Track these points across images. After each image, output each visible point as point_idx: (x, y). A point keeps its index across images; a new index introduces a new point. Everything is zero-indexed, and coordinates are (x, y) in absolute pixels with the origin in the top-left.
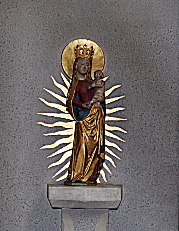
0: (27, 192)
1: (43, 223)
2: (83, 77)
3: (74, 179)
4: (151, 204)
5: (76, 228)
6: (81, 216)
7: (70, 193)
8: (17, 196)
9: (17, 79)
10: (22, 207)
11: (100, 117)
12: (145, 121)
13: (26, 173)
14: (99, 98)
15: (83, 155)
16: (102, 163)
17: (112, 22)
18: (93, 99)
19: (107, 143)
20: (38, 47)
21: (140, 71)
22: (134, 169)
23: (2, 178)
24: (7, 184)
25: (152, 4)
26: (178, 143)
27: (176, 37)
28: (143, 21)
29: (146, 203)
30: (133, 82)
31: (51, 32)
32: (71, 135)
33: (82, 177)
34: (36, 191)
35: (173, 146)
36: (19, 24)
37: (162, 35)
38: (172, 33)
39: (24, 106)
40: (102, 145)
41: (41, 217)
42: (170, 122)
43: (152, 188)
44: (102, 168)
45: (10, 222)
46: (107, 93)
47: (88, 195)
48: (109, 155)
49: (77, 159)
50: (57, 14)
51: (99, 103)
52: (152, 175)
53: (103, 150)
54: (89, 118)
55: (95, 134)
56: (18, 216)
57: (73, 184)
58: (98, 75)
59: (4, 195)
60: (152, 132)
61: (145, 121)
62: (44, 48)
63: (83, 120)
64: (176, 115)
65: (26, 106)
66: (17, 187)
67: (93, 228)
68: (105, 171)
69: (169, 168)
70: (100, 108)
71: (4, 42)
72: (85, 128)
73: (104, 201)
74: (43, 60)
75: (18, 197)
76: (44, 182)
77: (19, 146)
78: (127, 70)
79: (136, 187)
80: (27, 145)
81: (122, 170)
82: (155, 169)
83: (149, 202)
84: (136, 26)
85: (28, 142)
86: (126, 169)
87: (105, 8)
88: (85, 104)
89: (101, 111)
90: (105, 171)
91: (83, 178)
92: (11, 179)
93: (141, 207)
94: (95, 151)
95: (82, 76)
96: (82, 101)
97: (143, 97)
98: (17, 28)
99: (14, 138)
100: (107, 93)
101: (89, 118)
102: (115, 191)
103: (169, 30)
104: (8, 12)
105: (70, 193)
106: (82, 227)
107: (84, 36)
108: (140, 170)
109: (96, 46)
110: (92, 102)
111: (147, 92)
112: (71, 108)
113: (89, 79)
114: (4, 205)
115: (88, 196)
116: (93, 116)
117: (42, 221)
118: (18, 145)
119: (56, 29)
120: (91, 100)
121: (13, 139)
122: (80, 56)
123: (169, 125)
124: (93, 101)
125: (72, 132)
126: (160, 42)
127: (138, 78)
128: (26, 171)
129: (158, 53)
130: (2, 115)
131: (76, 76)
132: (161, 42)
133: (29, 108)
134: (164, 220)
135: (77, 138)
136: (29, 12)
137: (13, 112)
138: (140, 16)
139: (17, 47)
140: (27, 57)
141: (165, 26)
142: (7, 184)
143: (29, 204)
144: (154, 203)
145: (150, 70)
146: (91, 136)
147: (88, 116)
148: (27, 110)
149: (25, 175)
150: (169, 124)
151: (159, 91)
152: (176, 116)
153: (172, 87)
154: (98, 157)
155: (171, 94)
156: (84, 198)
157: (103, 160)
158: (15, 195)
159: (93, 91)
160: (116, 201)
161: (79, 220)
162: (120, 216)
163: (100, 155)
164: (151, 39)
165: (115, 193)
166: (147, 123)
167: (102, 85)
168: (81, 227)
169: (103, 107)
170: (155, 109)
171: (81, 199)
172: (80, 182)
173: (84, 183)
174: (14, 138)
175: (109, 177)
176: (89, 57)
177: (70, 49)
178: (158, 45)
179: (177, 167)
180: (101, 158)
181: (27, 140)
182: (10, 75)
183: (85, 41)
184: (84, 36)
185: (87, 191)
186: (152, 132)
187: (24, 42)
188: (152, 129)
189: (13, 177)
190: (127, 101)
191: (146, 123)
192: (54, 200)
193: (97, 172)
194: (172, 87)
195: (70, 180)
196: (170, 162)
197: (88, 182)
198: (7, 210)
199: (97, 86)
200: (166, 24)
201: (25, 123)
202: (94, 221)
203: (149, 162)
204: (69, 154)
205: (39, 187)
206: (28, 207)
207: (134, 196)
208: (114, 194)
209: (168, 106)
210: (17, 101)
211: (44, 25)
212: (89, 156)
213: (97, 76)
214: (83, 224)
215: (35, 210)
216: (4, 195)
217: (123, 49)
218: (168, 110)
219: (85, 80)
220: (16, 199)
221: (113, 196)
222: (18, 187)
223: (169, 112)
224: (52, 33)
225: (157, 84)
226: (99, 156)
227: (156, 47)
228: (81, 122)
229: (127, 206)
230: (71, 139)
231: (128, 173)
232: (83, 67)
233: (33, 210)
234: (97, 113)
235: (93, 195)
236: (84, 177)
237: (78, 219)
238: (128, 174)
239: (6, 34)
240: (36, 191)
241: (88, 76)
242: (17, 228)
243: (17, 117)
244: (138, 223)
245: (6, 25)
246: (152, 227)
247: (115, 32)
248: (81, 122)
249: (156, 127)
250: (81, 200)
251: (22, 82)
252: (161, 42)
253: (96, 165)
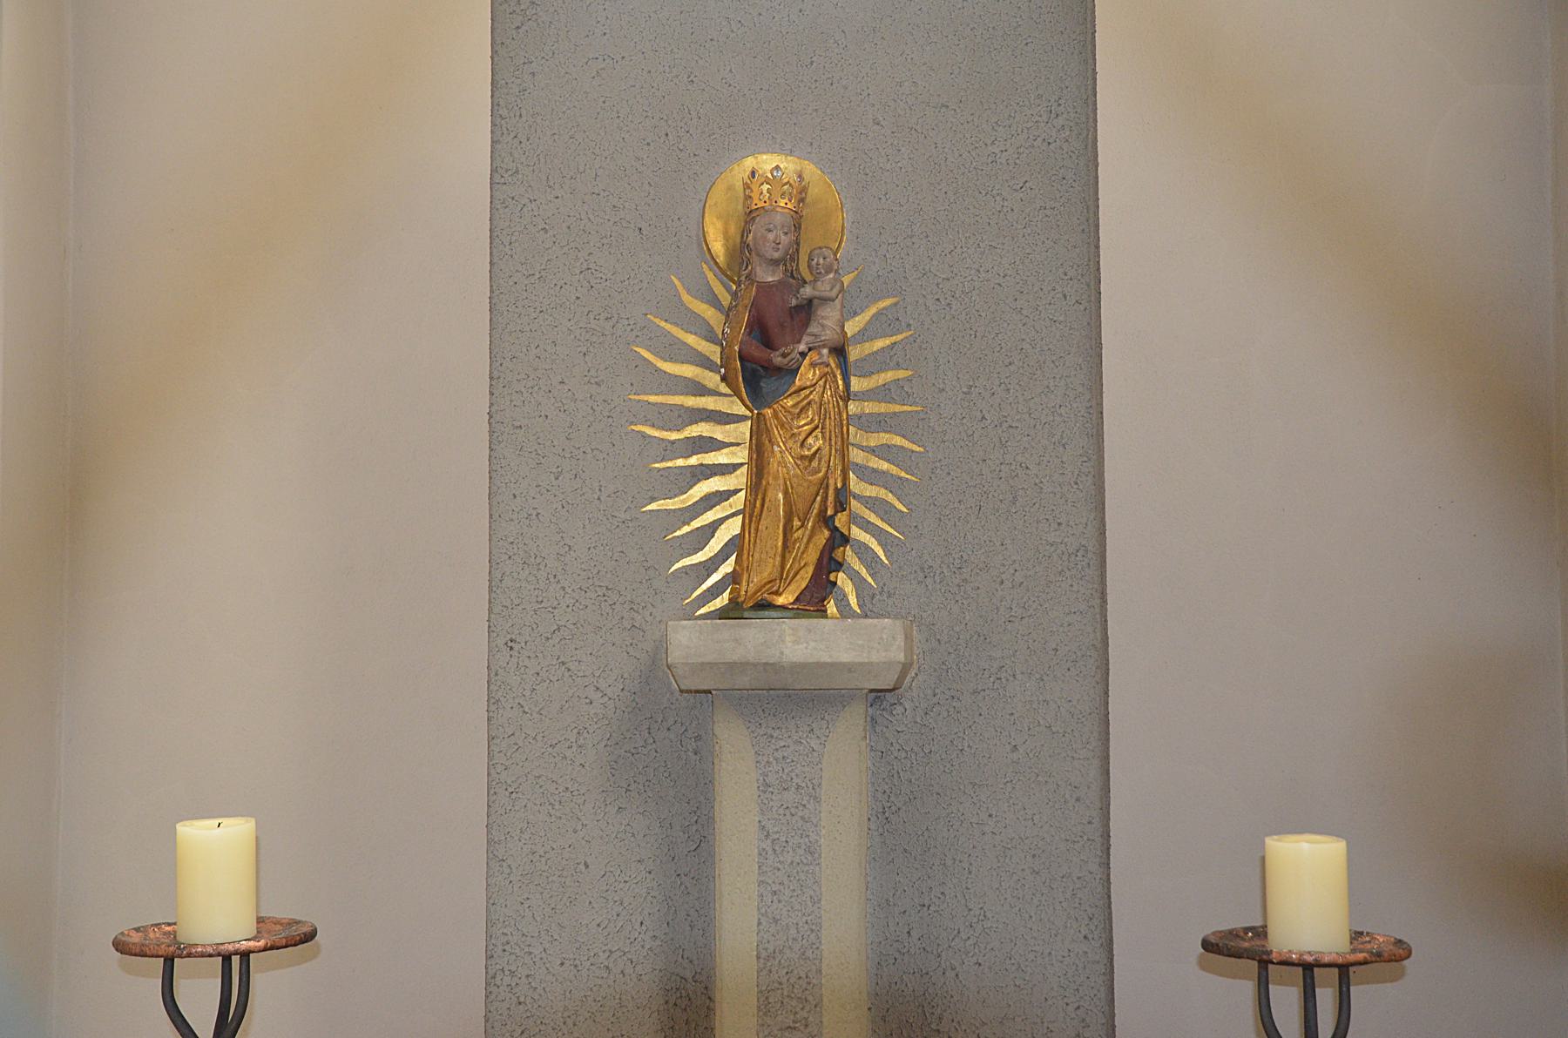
0: (600, 653)
1: (656, 752)
2: (774, 272)
3: (750, 599)
4: (1007, 680)
5: (760, 757)
6: (774, 716)
7: (736, 640)
8: (570, 665)
9: (561, 287)
10: (588, 701)
11: (831, 395)
12: (981, 411)
13: (598, 589)
14: (826, 335)
15: (778, 516)
16: (842, 548)
17: (865, 94)
18: (806, 339)
19: (855, 484)
20: (626, 185)
21: (959, 250)
22: (948, 566)
23: (520, 608)
24: (535, 626)
25: (994, 28)
26: (1091, 476)
27: (1076, 132)
28: (964, 87)
29: (992, 679)
30: (938, 284)
31: (667, 135)
32: (742, 489)
33: (775, 588)
34: (630, 649)
35: (1076, 486)
36: (999, 486)
37: (1028, 129)
38: (1061, 121)
39: (586, 373)
40: (839, 486)
41: (649, 733)
42: (1062, 411)
43: (1009, 626)
44: (839, 566)
45: (550, 749)
46: (851, 328)
47: (796, 642)
48: (867, 526)
49: (757, 530)
50: (686, 76)
51: (825, 351)
52: (1008, 584)
53: (841, 506)
54: (790, 403)
55: (814, 449)
56: (575, 731)
57: (746, 614)
58: (821, 261)
59: (527, 662)
60: (1003, 445)
61: (981, 411)
62: (647, 187)
63: (775, 406)
64: (1083, 385)
65: (593, 372)
66: (570, 637)
67: (815, 754)
68: (855, 577)
69: (1065, 557)
70: (828, 365)
71: (517, 172)
72: (781, 432)
73: (849, 663)
74: (644, 225)
75: (571, 668)
76: (658, 619)
77: (595, 451)
78: (916, 246)
79: (957, 629)
80: (599, 499)
81: (911, 573)
82: (1016, 566)
83: (1003, 675)
84: (943, 106)
85: (603, 489)
86: (922, 569)
87: (842, 51)
88: (777, 353)
89: (835, 376)
90: (855, 577)
91: (777, 593)
92: (550, 609)
93: (975, 692)
94: (817, 505)
95: (771, 268)
96: (768, 344)
97: (973, 333)
98: (556, 123)
99: (557, 479)
100: (851, 328)
101: (790, 403)
102: (885, 628)
103: (1051, 111)
104: (528, 72)
105: (736, 640)
106: (779, 755)
107: (776, 143)
108: (969, 569)
109: (811, 170)
110: (802, 347)
111: (983, 315)
112: (735, 369)
113: (793, 278)
114: (527, 693)
115: (796, 647)
116: (807, 392)
117: (654, 746)
118: (568, 499)
119: (682, 124)
120: (799, 342)
121: (554, 483)
122: (761, 204)
123: (1058, 419)
124: (807, 344)
125: (741, 455)
126: (1021, 150)
127: (955, 271)
128: (597, 583)
129: (1019, 187)
130: (515, 403)
131: (750, 268)
132: (1027, 151)
133: (603, 381)
134: (1054, 733)
135: (756, 467)
136: (594, 73)
137: (551, 395)
138: (956, 72)
139: (557, 186)
140: (592, 217)
141: (1040, 97)
142: (535, 626)
143: (609, 692)
144: (1019, 676)
145: (993, 244)
146: (802, 457)
147: (789, 393)
148: (595, 386)
149: (594, 596)
150: (1061, 415)
151: (1024, 312)
152: (1081, 390)
153: (1065, 296)
154: (827, 526)
155: (1061, 318)
156: (782, 653)
157: (845, 540)
158: (563, 663)
159: (805, 311)
160: (889, 664)
161: (770, 731)
162: (906, 725)
163: (833, 517)
164: (993, 143)
165: (885, 637)
166: (987, 416)
167: (835, 291)
168: (776, 754)
169: (839, 366)
170: (1012, 368)
171: (771, 655)
172: (763, 606)
173: (783, 607)
174: (557, 479)
175: (867, 599)
176: (789, 206)
177: (730, 188)
178: (1017, 161)
179: (1090, 555)
180: (836, 529)
181: (596, 485)
182: (538, 275)
183: (767, 162)
184: (776, 143)
185: (791, 632)
186: (1003, 445)
187: (581, 169)
188: (1004, 434)
189: (556, 603)
190: (920, 347)
191: (983, 418)
192: (687, 664)
193: (828, 577)
194: (1065, 296)
195: (737, 603)
196: (1066, 540)
197: (796, 607)
198: (537, 709)
199: (817, 293)
200: (1040, 92)
201: (591, 429)
202: (817, 732)
203: (998, 544)
204: (733, 527)
205: (642, 634)
206: (606, 699)
207: (953, 656)
208: (881, 638)
209: (1054, 358)
210: (563, 360)
211: (645, 114)
212: (796, 523)
213: (818, 264)
214: (782, 744)
215: (630, 709)
216: (527, 662)
217: (881, 185)
218: (1056, 371)
219: (779, 282)
220: (567, 674)
221: (876, 645)
222: (572, 635)
223: (1058, 377)
224: (670, 137)
225: (1018, 287)
226: (830, 523)
227: (1011, 168)
228: (768, 412)
229: (929, 692)
230: (738, 480)
231: (929, 580)
232: (771, 236)
233: (624, 709)
234: (821, 383)
235: (812, 644)
236: (781, 590)
237: (767, 727)
238: (930, 587)
239: (523, 145)
240: (630, 649)
241: (790, 269)
242: (570, 768)
243: (565, 411)
244: (969, 746)
245: (521, 116)
246: (1015, 756)
247: (876, 127)
248: (768, 412)
249: (1017, 427)
250: (771, 662)
251: (578, 298)
252: (1027, 151)
253: (822, 553)
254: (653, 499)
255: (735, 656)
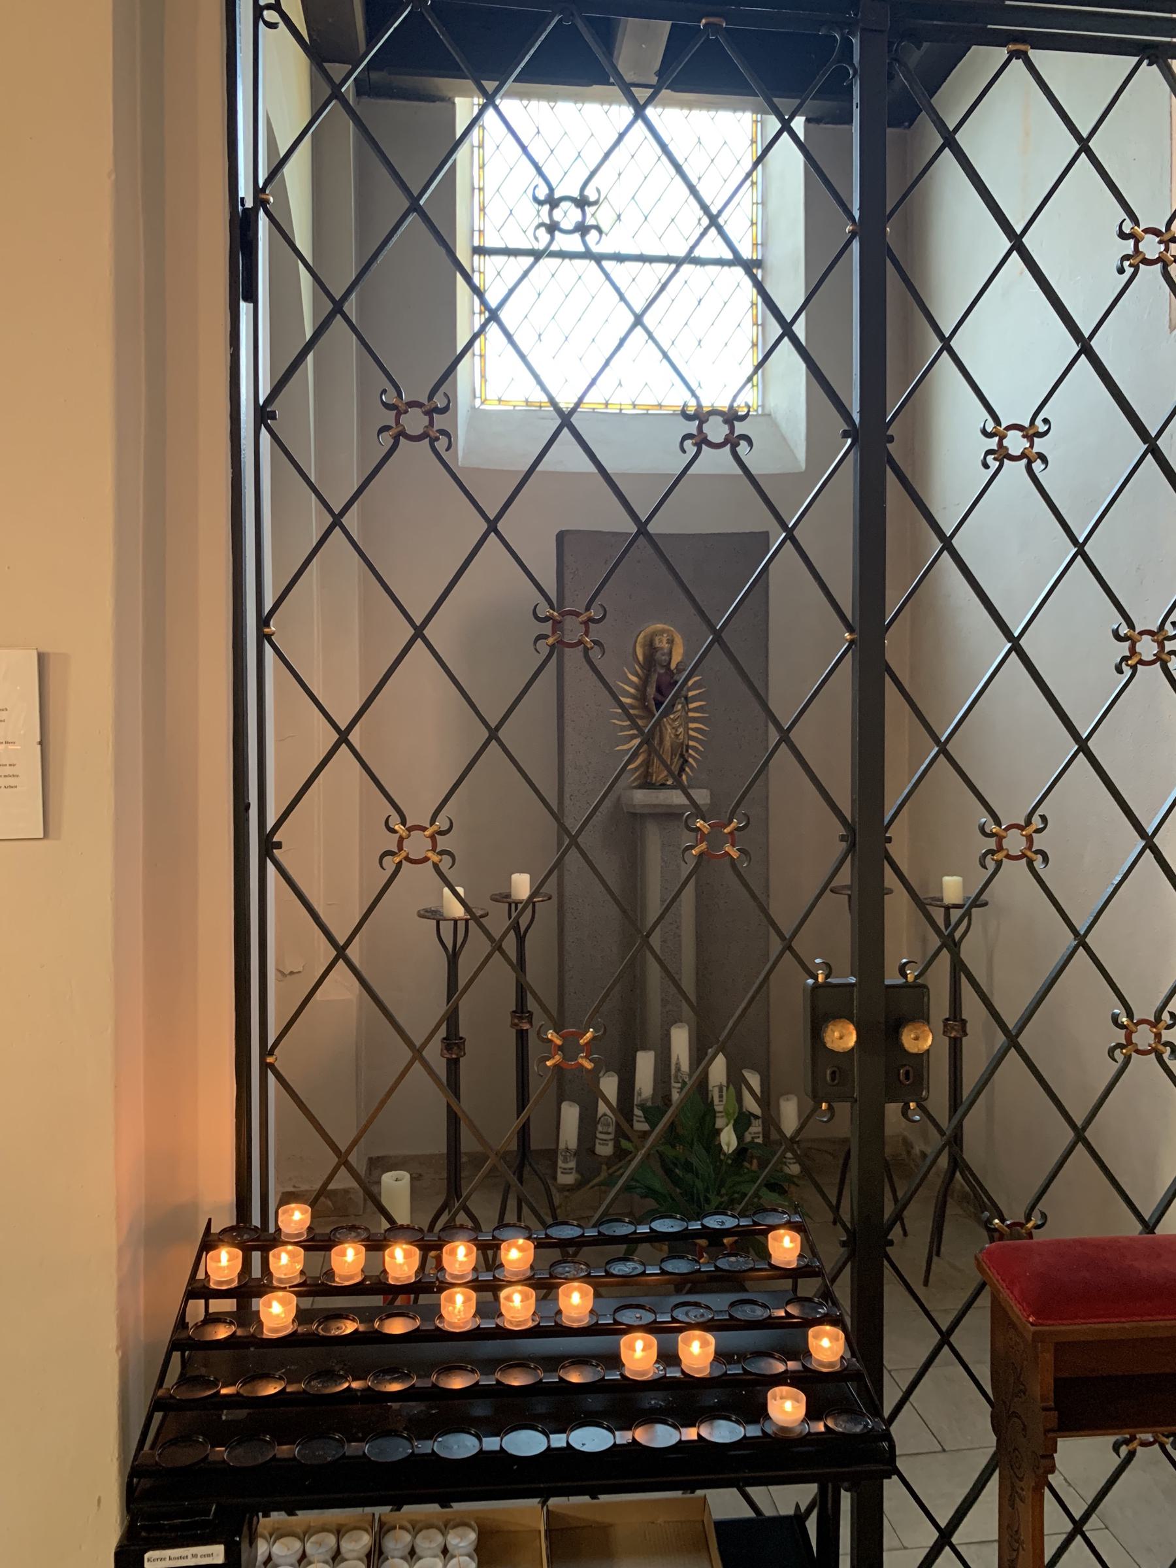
171: (668, 802)
254: (618, 746)
255: (656, 802)
